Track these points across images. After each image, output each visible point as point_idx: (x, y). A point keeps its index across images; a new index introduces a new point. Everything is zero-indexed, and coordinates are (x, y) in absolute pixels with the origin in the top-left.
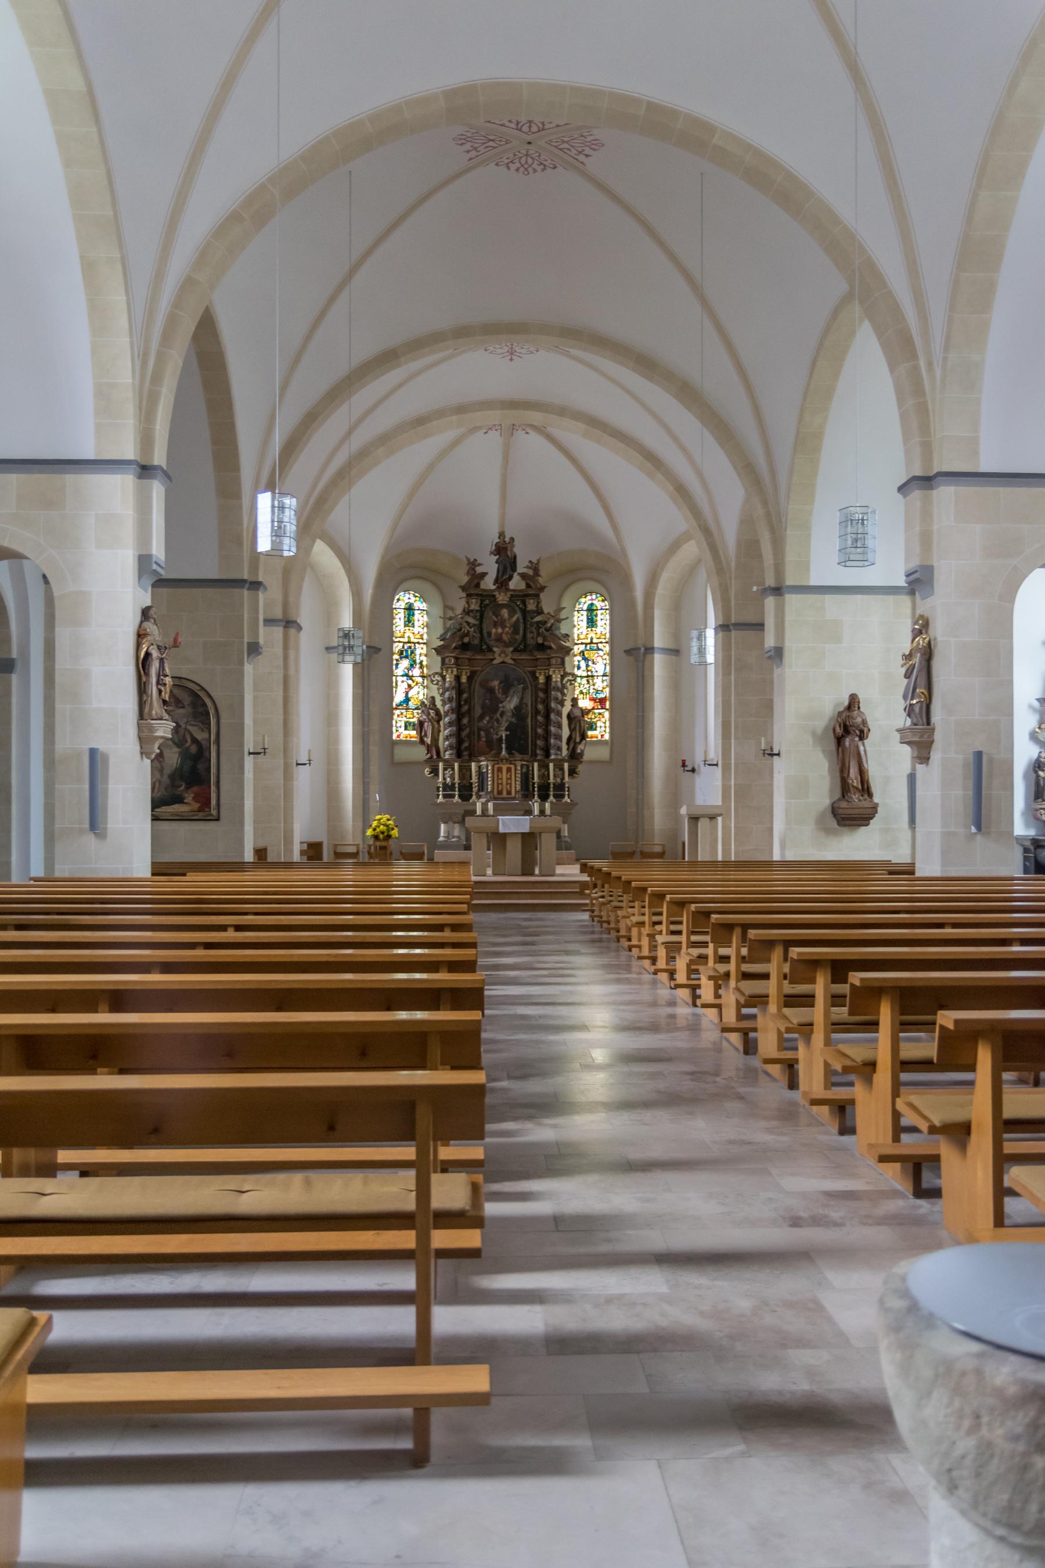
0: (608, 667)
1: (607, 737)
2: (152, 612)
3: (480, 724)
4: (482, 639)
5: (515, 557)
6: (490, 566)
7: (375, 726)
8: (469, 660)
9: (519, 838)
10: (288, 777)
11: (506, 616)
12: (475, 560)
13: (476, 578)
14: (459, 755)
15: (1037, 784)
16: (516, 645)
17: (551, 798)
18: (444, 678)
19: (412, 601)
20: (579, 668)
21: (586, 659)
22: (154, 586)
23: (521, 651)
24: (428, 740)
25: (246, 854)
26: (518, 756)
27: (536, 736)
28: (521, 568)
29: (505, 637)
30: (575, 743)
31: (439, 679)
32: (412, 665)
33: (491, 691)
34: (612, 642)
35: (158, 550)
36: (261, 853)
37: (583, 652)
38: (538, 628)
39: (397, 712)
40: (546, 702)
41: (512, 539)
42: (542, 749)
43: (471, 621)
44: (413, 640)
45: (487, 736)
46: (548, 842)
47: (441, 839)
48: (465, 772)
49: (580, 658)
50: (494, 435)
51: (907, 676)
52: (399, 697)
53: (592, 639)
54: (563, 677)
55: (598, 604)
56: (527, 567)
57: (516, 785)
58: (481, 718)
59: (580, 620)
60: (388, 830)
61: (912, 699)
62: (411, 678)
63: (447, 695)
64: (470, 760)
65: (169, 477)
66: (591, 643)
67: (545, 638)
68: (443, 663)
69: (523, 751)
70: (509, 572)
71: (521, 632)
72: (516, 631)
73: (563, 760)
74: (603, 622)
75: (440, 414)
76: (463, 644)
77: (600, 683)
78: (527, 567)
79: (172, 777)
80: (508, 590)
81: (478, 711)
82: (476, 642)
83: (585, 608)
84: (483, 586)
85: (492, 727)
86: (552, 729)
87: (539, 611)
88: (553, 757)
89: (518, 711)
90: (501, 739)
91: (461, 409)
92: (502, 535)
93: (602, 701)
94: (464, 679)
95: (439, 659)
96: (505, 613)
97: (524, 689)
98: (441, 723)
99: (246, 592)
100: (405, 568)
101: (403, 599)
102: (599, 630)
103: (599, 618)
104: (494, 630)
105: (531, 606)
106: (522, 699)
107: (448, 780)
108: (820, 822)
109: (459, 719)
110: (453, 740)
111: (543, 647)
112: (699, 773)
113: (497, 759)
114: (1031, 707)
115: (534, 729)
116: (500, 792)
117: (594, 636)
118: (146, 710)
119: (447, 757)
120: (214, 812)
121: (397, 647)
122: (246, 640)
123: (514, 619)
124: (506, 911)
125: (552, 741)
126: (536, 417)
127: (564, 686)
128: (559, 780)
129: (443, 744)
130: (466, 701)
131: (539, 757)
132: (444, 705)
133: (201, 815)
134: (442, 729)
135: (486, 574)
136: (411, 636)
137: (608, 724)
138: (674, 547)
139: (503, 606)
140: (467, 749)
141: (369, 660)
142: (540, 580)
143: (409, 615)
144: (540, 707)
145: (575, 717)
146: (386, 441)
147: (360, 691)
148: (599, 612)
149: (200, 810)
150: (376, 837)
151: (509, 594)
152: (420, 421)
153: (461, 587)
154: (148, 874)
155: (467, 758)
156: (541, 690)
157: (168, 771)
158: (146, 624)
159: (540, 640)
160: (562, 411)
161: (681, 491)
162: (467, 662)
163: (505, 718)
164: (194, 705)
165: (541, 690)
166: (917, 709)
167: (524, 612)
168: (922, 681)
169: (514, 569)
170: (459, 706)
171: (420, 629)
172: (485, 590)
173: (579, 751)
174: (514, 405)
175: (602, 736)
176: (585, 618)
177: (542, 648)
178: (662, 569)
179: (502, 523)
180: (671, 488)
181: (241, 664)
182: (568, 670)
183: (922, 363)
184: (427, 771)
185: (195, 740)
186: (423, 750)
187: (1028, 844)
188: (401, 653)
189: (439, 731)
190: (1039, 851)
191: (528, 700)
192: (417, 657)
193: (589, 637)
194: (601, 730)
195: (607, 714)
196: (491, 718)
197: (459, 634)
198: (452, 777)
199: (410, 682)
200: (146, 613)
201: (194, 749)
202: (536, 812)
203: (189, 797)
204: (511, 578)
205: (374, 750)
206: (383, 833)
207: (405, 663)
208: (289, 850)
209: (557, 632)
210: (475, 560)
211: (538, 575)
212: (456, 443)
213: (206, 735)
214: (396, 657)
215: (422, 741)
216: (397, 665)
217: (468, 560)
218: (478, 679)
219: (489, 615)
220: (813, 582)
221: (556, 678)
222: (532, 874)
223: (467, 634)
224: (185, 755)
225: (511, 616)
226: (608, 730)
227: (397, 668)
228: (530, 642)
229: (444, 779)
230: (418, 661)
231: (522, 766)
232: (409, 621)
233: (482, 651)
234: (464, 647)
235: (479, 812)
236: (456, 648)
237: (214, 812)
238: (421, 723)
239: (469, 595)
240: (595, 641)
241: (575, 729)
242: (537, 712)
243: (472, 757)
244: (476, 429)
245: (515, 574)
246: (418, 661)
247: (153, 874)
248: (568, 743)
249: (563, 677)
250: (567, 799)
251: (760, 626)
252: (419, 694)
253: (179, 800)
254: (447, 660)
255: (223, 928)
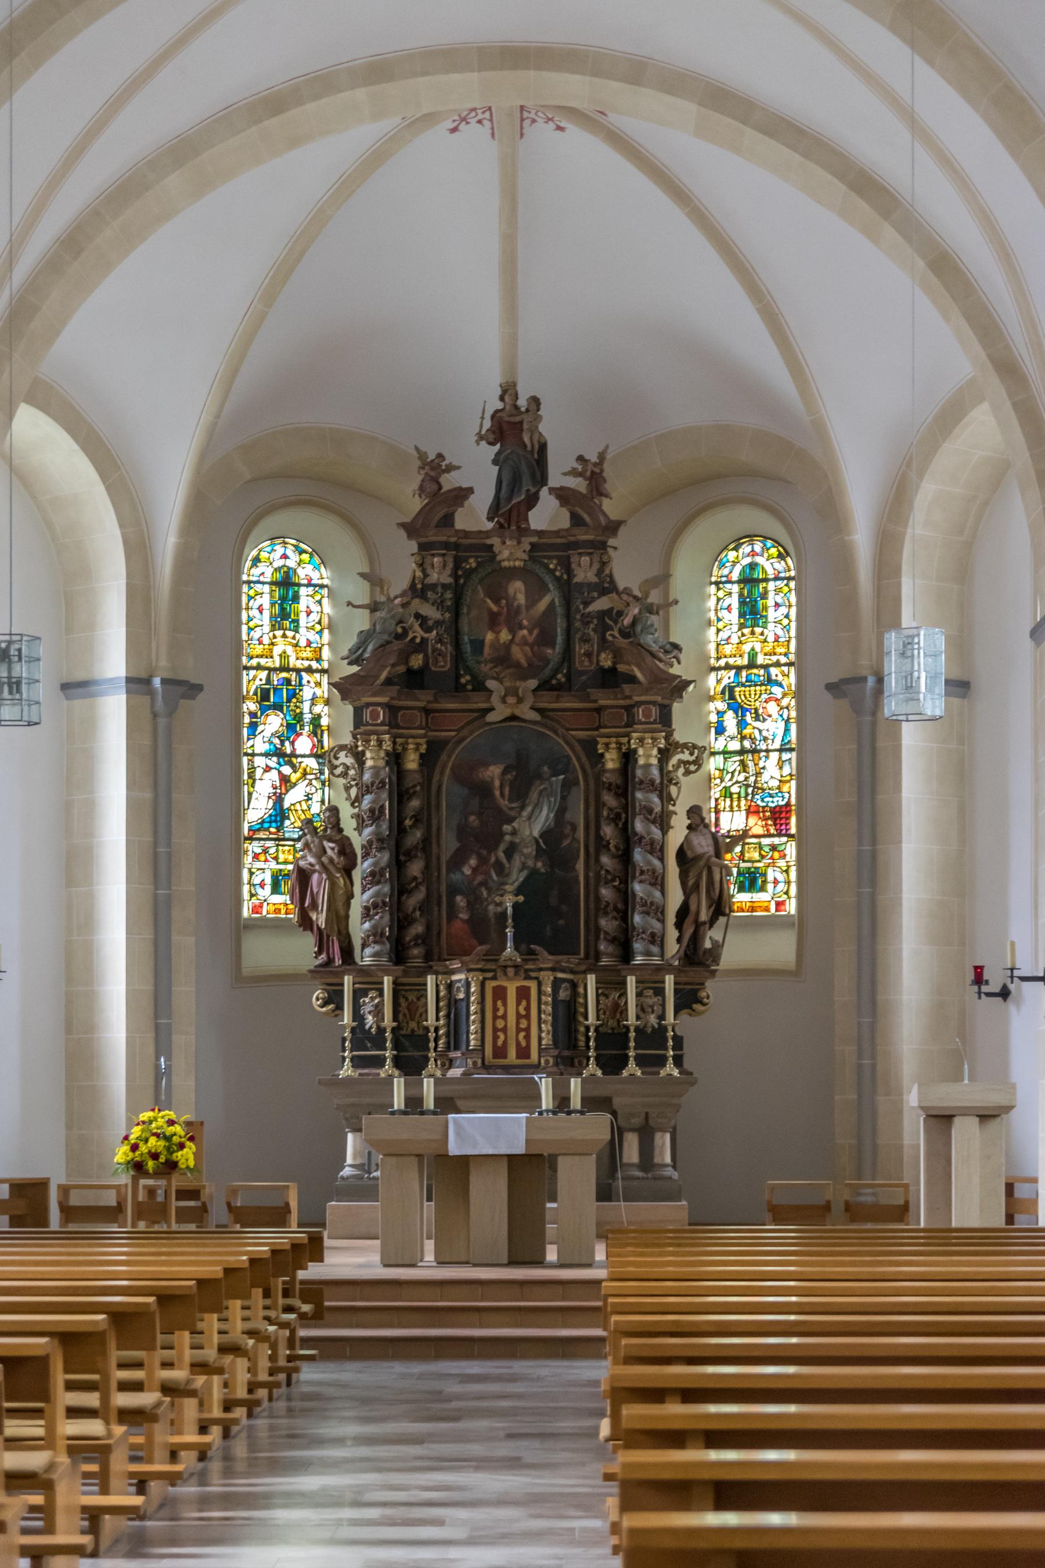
0: (793, 728)
3: (456, 877)
4: (458, 657)
5: (543, 447)
6: (478, 471)
7: (186, 882)
8: (427, 711)
9: (504, 1166)
11: (521, 599)
12: (440, 456)
13: (442, 500)
14: (399, 955)
16: (547, 671)
17: (632, 1065)
19: (291, 563)
20: (720, 730)
21: (739, 709)
23: (559, 688)
24: (320, 919)
26: (547, 959)
27: (599, 908)
28: (556, 478)
29: (518, 654)
30: (698, 925)
31: (350, 761)
32: (290, 727)
33: (483, 790)
34: (799, 664)
37: (731, 689)
38: (603, 628)
39: (255, 847)
41: (535, 401)
42: (613, 940)
44: (293, 662)
45: (470, 905)
46: (577, 1177)
47: (347, 1171)
48: (408, 1001)
49: (721, 706)
50: (475, 133)
52: (258, 808)
53: (753, 655)
54: (664, 755)
55: (769, 564)
56: (573, 473)
57: (542, 1034)
58: (457, 861)
59: (723, 606)
60: (169, 1150)
63: (367, 800)
64: (423, 973)
66: (752, 665)
67: (618, 655)
68: (358, 722)
69: (561, 943)
70: (527, 485)
71: (560, 639)
72: (546, 638)
73: (667, 968)
74: (781, 608)
75: (324, 84)
76: (410, 671)
78: (573, 473)
80: (524, 531)
81: (449, 843)
82: (445, 665)
83: (735, 576)
84: (461, 522)
85: (484, 884)
86: (638, 888)
87: (606, 586)
88: (639, 960)
89: (551, 842)
90: (504, 914)
91: (378, 72)
92: (508, 391)
93: (778, 816)
94: (412, 762)
95: (349, 709)
96: (517, 589)
97: (568, 786)
98: (357, 875)
100: (263, 476)
101: (268, 559)
102: (772, 631)
103: (302, 605)
104: (490, 636)
105: (584, 571)
106: (560, 813)
107: (370, 1020)
109: (399, 864)
110: (382, 918)
111: (613, 675)
112: (1018, 1004)
113: (491, 966)
116: (500, 1052)
117: (758, 647)
119: (368, 961)
121: (253, 681)
123: (543, 605)
124: (438, 1356)
125: (637, 919)
126: (572, 87)
127: (668, 779)
128: (653, 1019)
129: (358, 928)
130: (417, 819)
131: (605, 961)
132: (359, 829)
134: (357, 888)
135: (470, 491)
136: (290, 650)
137: (793, 875)
138: (949, 417)
139: (512, 573)
141: (171, 713)
142: (607, 505)
143: (283, 599)
144: (608, 831)
145: (698, 858)
146: (189, 155)
147: (148, 795)
148: (771, 586)
150: (138, 1167)
151: (526, 543)
152: (274, 103)
153: (403, 525)
155: (418, 962)
156: (609, 788)
160: (636, 71)
161: (944, 269)
162: (419, 718)
163: (517, 861)
165: (609, 788)
167: (568, 589)
170: (400, 830)
171: (313, 636)
172: (467, 534)
173: (708, 944)
174: (513, 57)
175: (779, 905)
176: (734, 601)
177: (611, 678)
178: (921, 475)
179: (510, 361)
180: (921, 264)
184: (318, 994)
186: (308, 942)
188: (265, 695)
189: (352, 896)
191: (578, 814)
192: (306, 707)
193: (746, 648)
194: (775, 887)
195: (791, 850)
196: (483, 861)
197: (397, 645)
198: (378, 1011)
199: (287, 770)
202: (546, 1101)
204: (532, 501)
205: (185, 944)
206: (155, 1156)
209: (648, 640)
210: (440, 456)
211: (602, 494)
212: (376, 158)
214: (251, 706)
215: (306, 922)
216: (253, 726)
217: (422, 456)
218: (449, 761)
219: (479, 599)
221: (647, 756)
222: (539, 1262)
225: (532, 602)
226: (793, 890)
227: (253, 734)
228: (582, 664)
230: (307, 717)
231: (556, 984)
232: (284, 615)
233: (459, 688)
234: (414, 680)
235: (398, 1101)
236: (388, 682)
238: (303, 876)
239: (423, 547)
240: (760, 660)
241: (697, 886)
242: (602, 845)
243: (434, 959)
244: (429, 119)
245: (544, 492)
246: (307, 717)
248: (679, 925)
249: (664, 755)
250: (671, 1069)
252: (307, 799)
254: (367, 715)
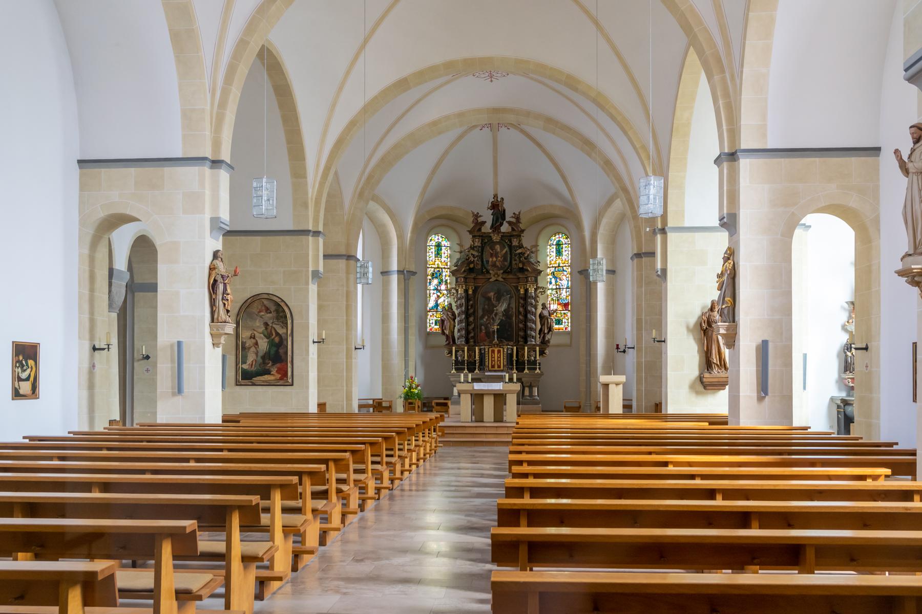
1: (569, 329)
2: (219, 254)
4: (483, 265)
6: (488, 217)
10: (349, 357)
13: (479, 224)
14: (467, 342)
15: (846, 361)
18: (457, 291)
20: (551, 283)
21: (555, 278)
22: (224, 235)
23: (508, 273)
25: (310, 408)
29: (498, 264)
33: (489, 299)
35: (225, 215)
36: (322, 406)
39: (430, 313)
40: (525, 306)
41: (502, 199)
43: (476, 253)
51: (720, 289)
52: (431, 304)
54: (536, 290)
55: (563, 240)
58: (482, 317)
59: (551, 251)
61: (723, 304)
62: (439, 291)
65: (232, 168)
67: (524, 264)
68: (457, 282)
69: (509, 339)
70: (500, 220)
72: (505, 260)
77: (564, 294)
79: (263, 358)
81: (480, 313)
82: (479, 267)
84: (483, 230)
92: (495, 196)
93: (566, 305)
94: (470, 292)
96: (498, 247)
97: (511, 298)
99: (310, 238)
100: (434, 220)
102: (564, 257)
105: (515, 243)
106: (509, 305)
108: (692, 387)
109: (467, 318)
111: (522, 269)
114: (843, 307)
115: (517, 325)
118: (216, 317)
120: (290, 381)
121: (430, 271)
122: (311, 269)
129: (456, 335)
133: (281, 382)
140: (473, 337)
144: (521, 309)
149: (281, 379)
154: (220, 422)
157: (261, 354)
158: (215, 262)
159: (521, 266)
164: (277, 311)
166: (726, 312)
167: (510, 247)
168: (729, 293)
169: (504, 219)
170: (467, 309)
181: (307, 284)
182: (540, 285)
183: (728, 76)
185: (277, 334)
186: (444, 338)
187: (839, 402)
188: (433, 275)
190: (847, 407)
195: (569, 314)
200: (216, 255)
201: (277, 340)
203: (274, 371)
204: (501, 224)
207: (435, 282)
208: (349, 404)
213: (285, 331)
214: (429, 277)
215: (443, 333)
219: (487, 248)
220: (687, 224)
221: (532, 290)
223: (473, 262)
224: (271, 344)
225: (502, 250)
228: (514, 266)
229: (456, 357)
234: (471, 270)
237: (290, 381)
238: (442, 321)
242: (520, 313)
247: (223, 421)
250: (538, 370)
251: (652, 254)
252: (444, 301)
253: (268, 372)
255: (187, 460)
